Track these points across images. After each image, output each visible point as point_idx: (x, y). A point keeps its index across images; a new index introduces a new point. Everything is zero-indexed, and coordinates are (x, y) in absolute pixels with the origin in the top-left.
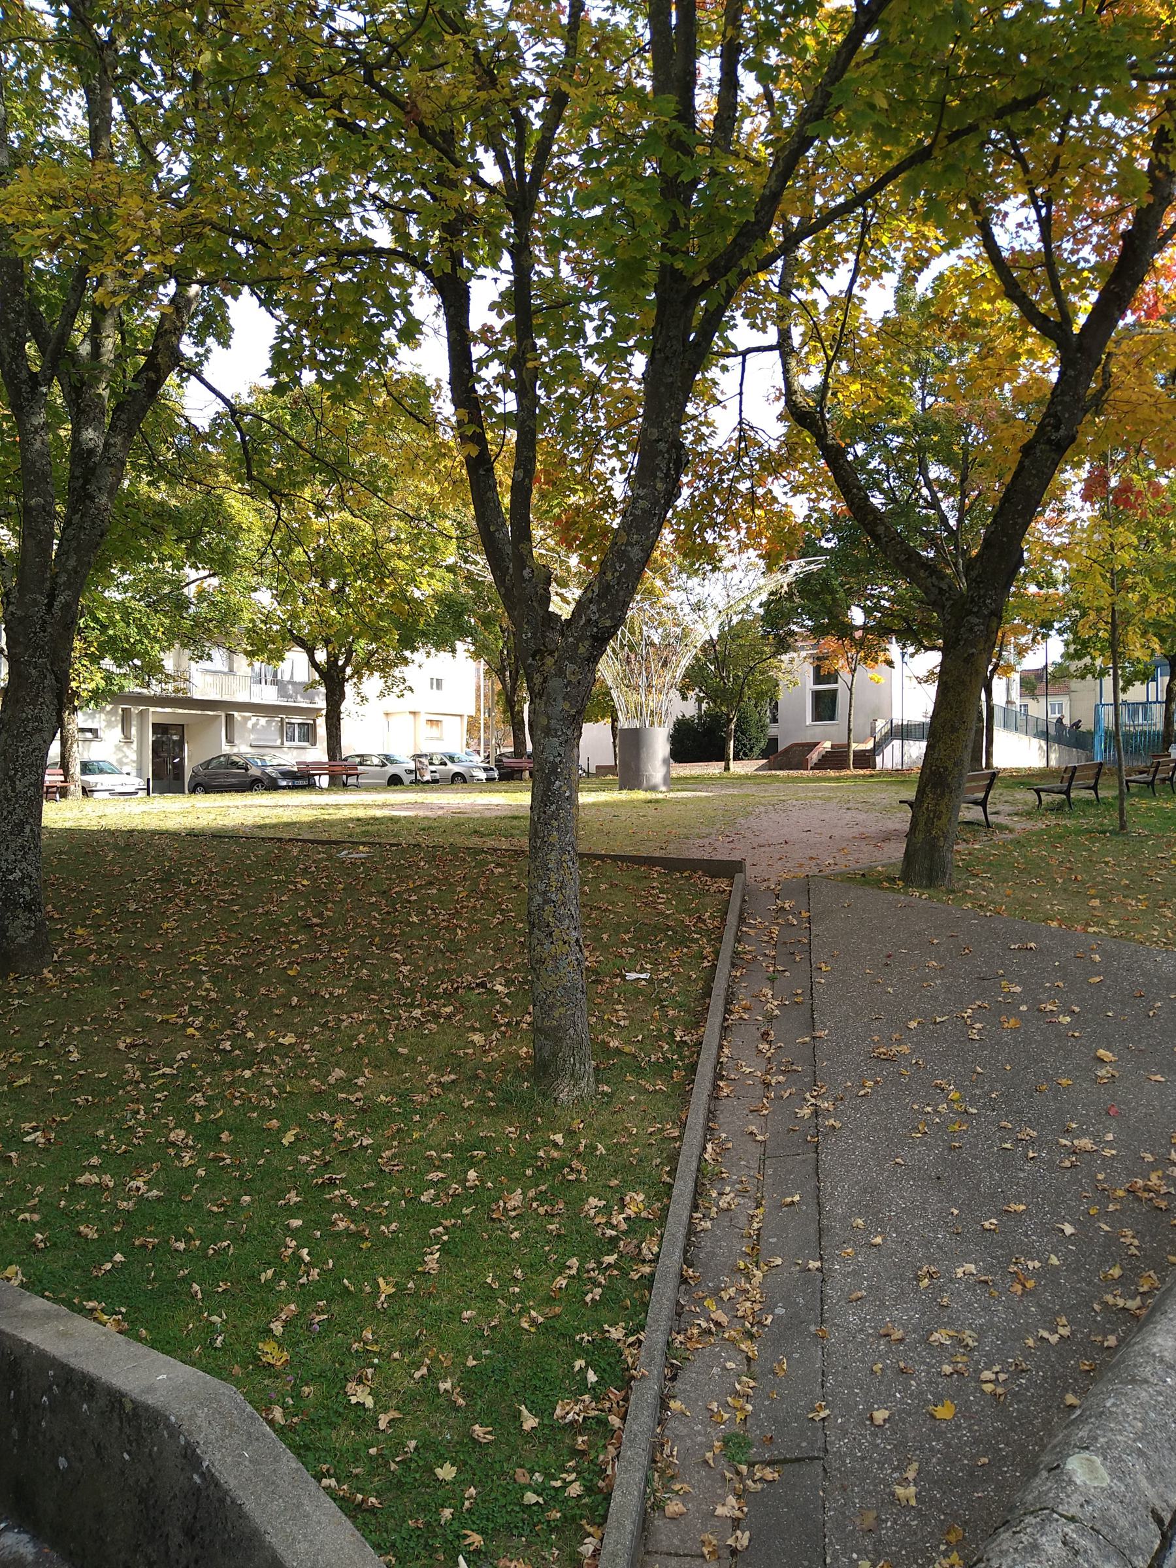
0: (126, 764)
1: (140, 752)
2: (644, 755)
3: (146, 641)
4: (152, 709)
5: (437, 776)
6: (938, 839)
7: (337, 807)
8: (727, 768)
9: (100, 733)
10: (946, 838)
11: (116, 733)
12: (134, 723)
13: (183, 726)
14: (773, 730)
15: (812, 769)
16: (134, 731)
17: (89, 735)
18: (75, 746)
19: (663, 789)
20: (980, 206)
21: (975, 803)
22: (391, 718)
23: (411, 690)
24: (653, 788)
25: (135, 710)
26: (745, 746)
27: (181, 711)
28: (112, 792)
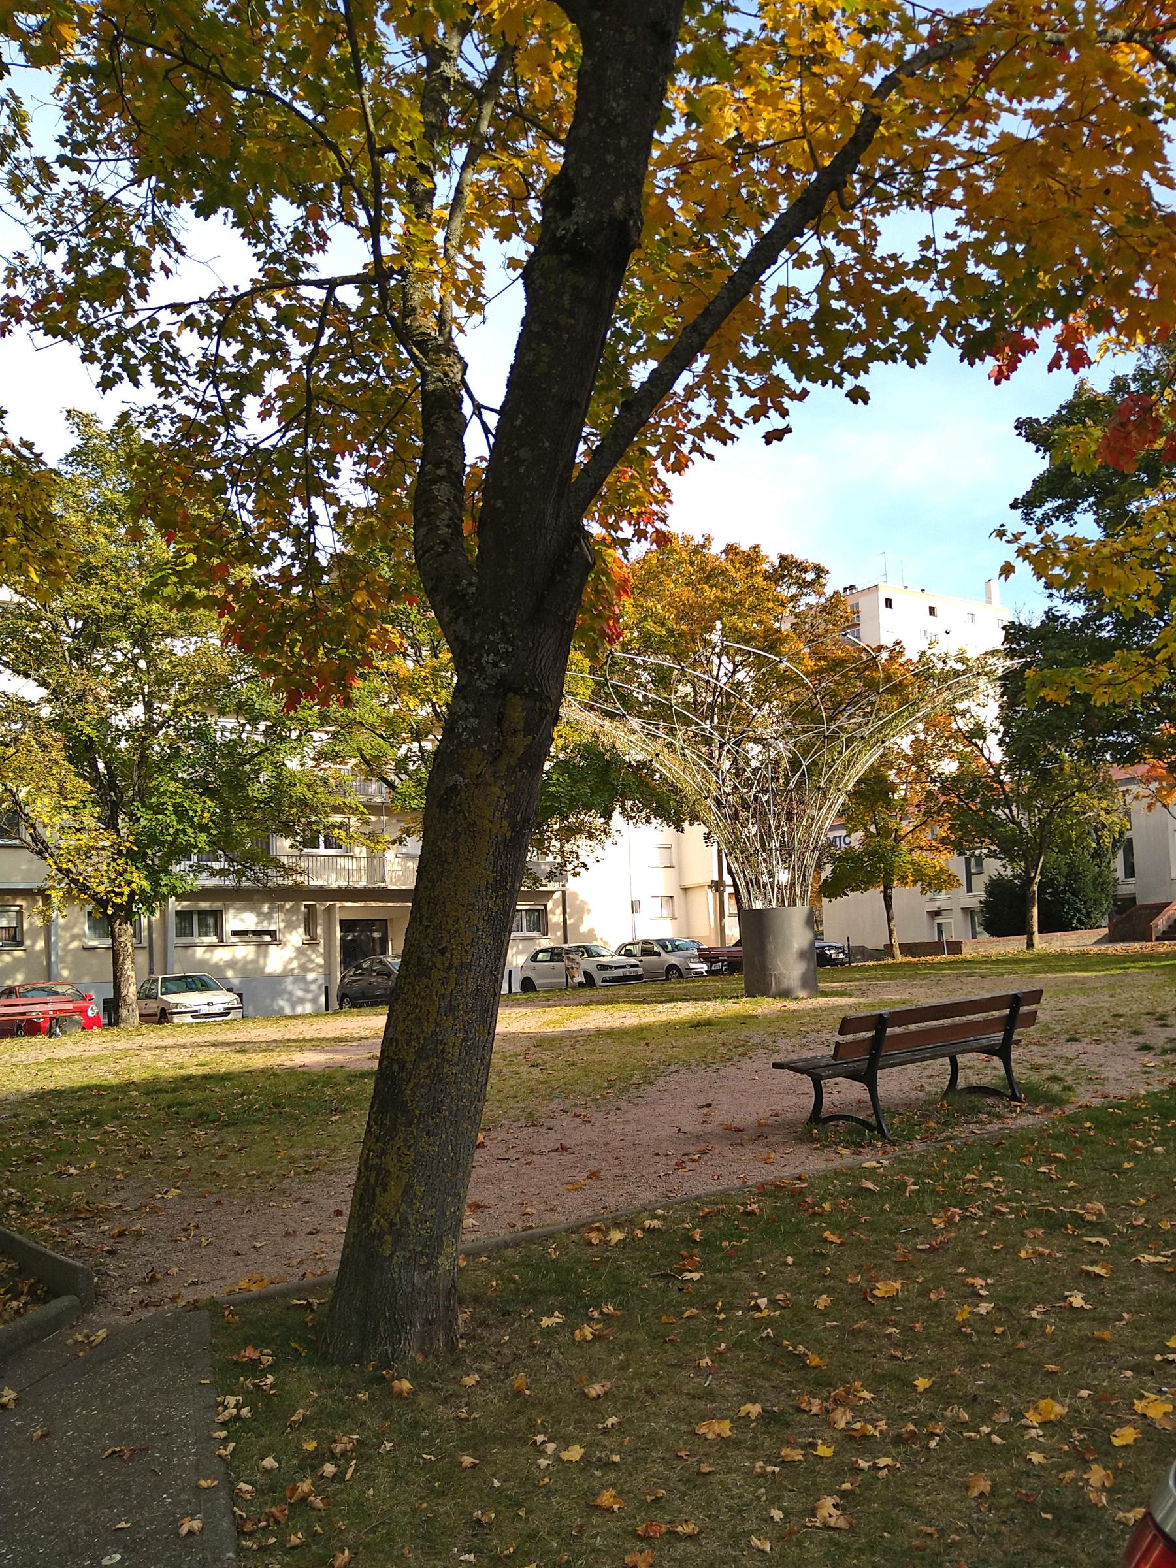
0: (311, 970)
1: (327, 956)
2: (770, 947)
3: (190, 831)
4: (338, 904)
5: (640, 971)
6: (379, 1236)
7: (242, 1048)
8: (1030, 945)
9: (279, 936)
10: (398, 1236)
11: (297, 937)
12: (320, 921)
13: (385, 921)
14: (1126, 888)
15: (1158, 939)
16: (319, 931)
17: (267, 938)
18: (128, 961)
19: (802, 994)
20: (1114, 78)
21: (989, 1051)
22: (691, 894)
23: (585, 866)
24: (786, 994)
25: (321, 907)
26: (1078, 910)
27: (373, 904)
28: (195, 1014)
